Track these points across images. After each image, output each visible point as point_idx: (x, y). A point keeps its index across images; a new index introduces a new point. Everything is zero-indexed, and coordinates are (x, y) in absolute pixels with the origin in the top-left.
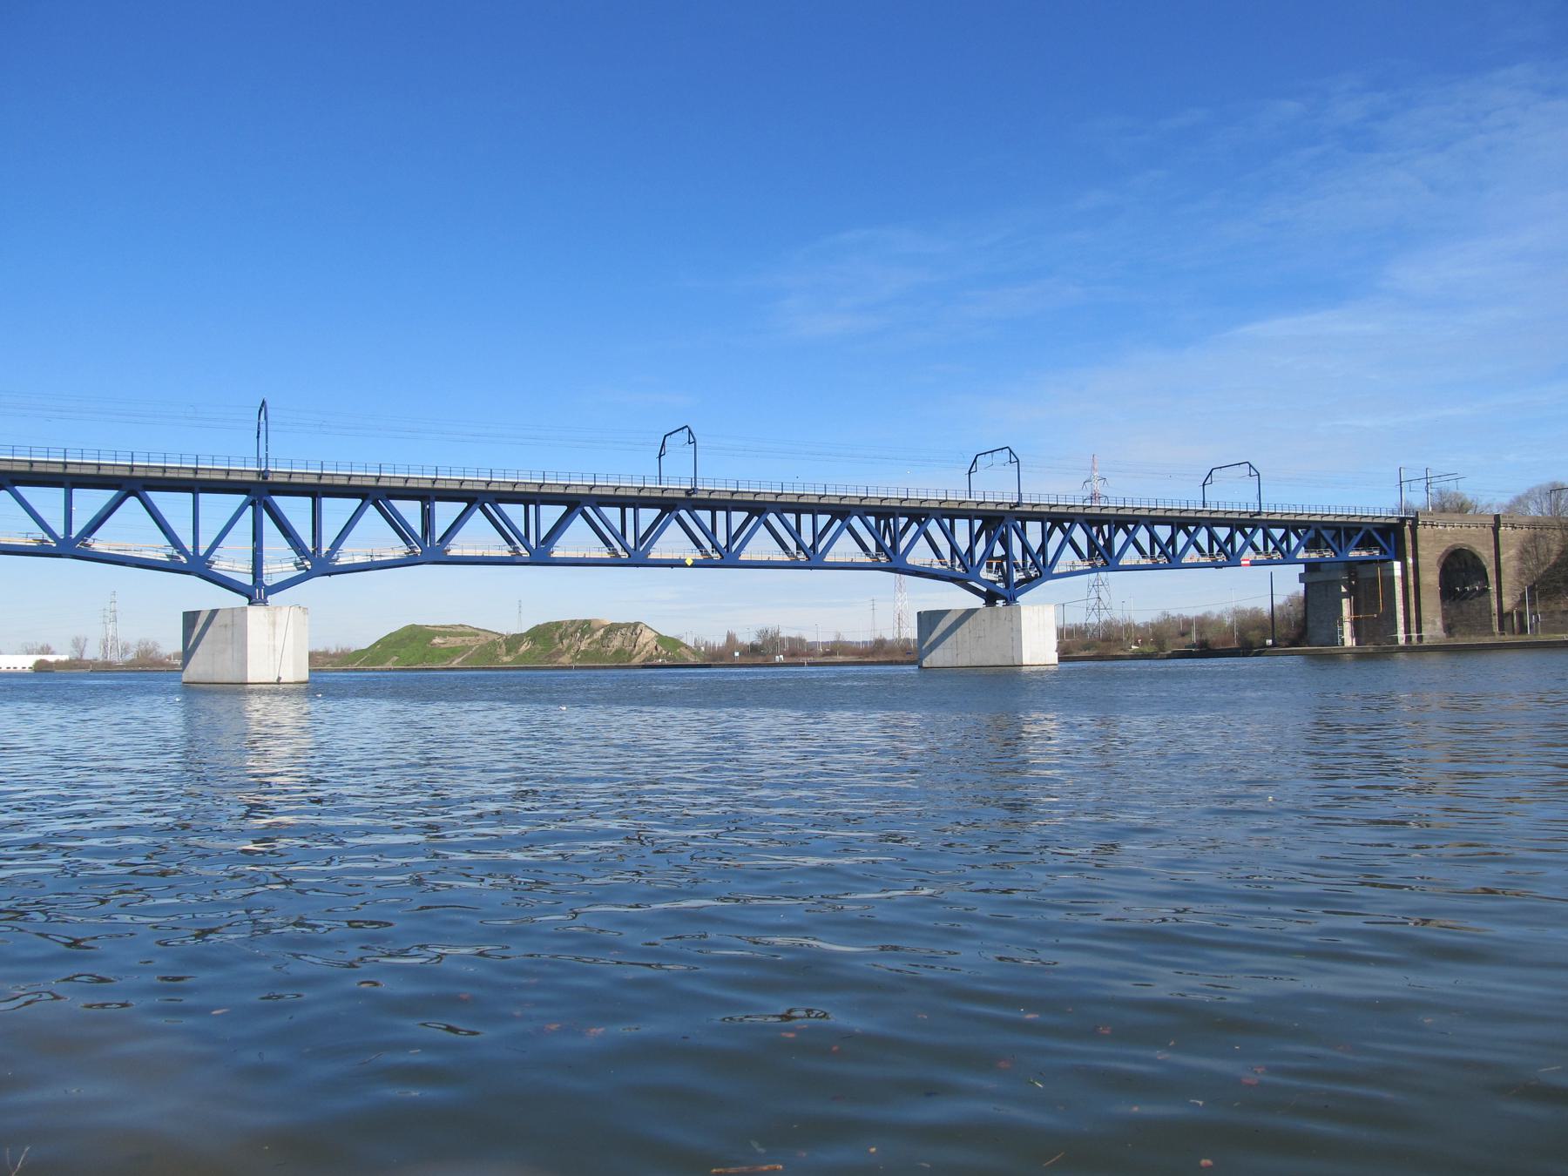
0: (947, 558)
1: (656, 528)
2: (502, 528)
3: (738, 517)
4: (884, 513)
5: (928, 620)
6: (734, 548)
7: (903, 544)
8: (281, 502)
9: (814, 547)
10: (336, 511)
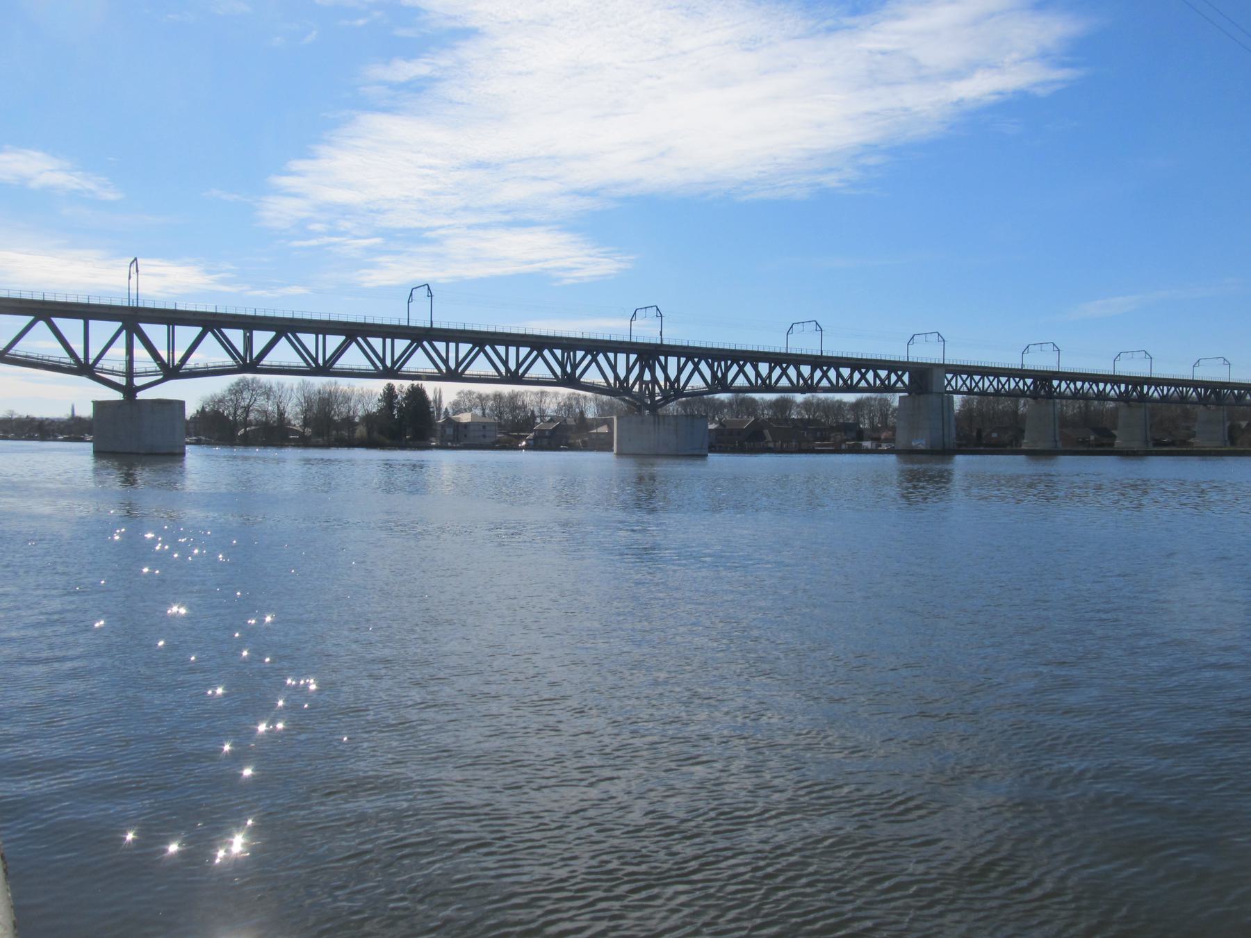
0: (612, 381)
1: (407, 354)
2: (300, 349)
4: (569, 345)
7: (578, 372)
8: (145, 327)
10: (185, 335)
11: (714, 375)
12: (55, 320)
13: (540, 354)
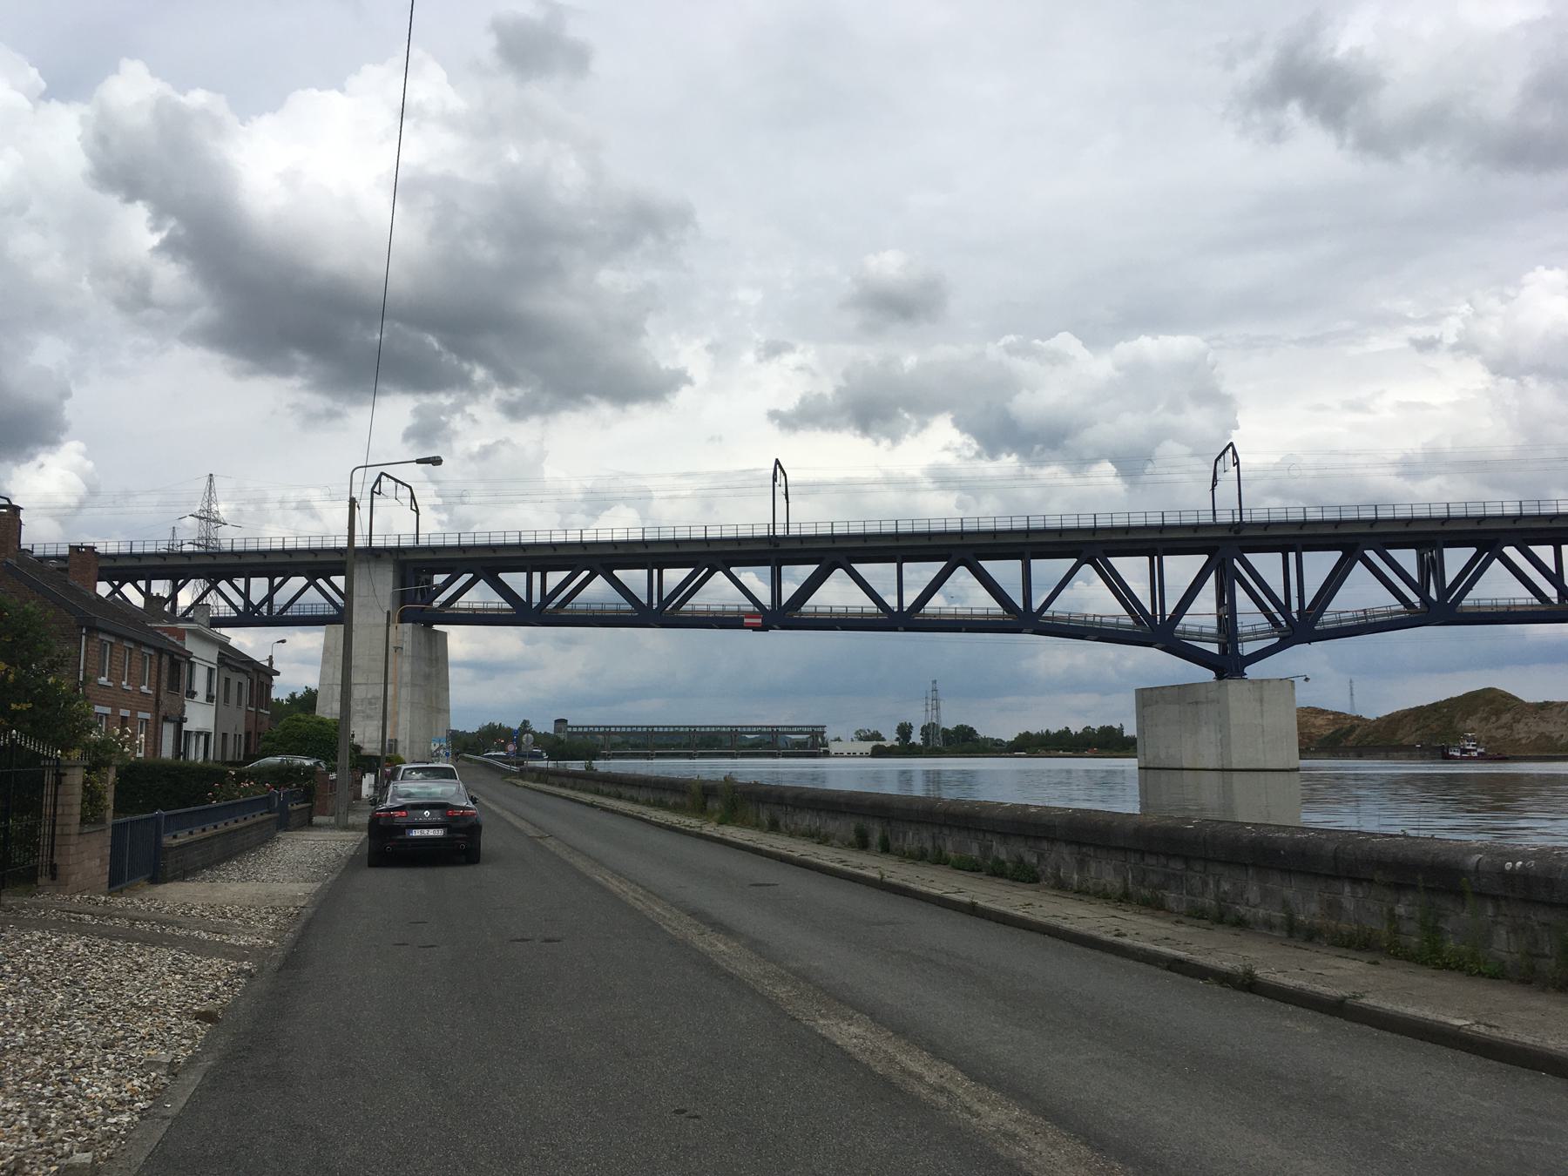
5: (1148, 699)
12: (987, 565)
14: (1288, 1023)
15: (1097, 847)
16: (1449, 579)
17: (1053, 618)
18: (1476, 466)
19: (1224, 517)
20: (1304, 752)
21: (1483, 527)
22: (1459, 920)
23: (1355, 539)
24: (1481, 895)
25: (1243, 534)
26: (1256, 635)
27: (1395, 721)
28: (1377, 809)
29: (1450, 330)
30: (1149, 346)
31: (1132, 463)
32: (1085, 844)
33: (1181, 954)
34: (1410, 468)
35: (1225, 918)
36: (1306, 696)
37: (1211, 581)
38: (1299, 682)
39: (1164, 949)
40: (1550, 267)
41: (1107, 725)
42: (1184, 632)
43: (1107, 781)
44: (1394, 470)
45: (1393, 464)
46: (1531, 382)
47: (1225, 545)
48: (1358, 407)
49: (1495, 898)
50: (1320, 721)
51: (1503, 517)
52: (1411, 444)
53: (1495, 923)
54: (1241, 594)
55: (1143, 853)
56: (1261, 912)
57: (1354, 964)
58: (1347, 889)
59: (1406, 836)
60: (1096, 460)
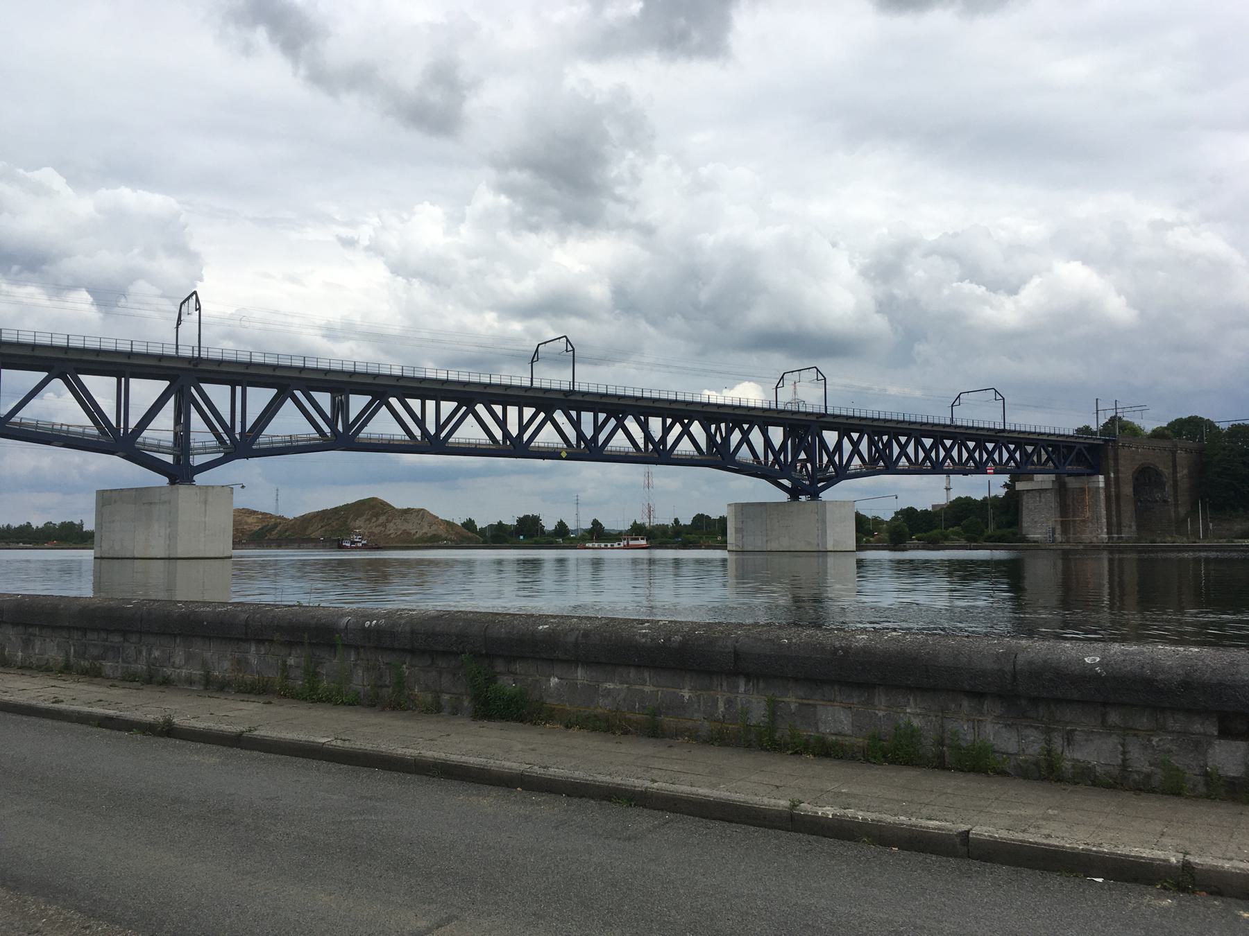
1: (367, 415)
3: (448, 407)
5: (107, 499)
6: (443, 435)
9: (595, 437)
11: (710, 438)
13: (550, 418)
14: (196, 758)
15: (42, 627)
16: (352, 417)
17: (20, 424)
18: (376, 337)
19: (186, 352)
20: (237, 544)
21: (377, 381)
22: (332, 664)
23: (289, 381)
24: (347, 646)
25: (200, 367)
26: (205, 450)
27: (306, 520)
28: (290, 586)
29: (364, 234)
30: (129, 197)
31: (108, 295)
32: (32, 626)
33: (111, 712)
34: (331, 333)
35: (155, 679)
36: (242, 500)
37: (171, 403)
38: (237, 489)
39: (98, 710)
40: (432, 204)
41: (68, 520)
42: (144, 444)
43: (67, 570)
44: (320, 332)
45: (320, 327)
46: (416, 282)
47: (185, 375)
48: (294, 279)
49: (357, 648)
50: (251, 520)
51: (391, 376)
52: (334, 314)
53: (355, 665)
54: (195, 416)
55: (84, 630)
56: (184, 672)
57: (252, 706)
58: (253, 649)
59: (300, 606)
60: (74, 287)
